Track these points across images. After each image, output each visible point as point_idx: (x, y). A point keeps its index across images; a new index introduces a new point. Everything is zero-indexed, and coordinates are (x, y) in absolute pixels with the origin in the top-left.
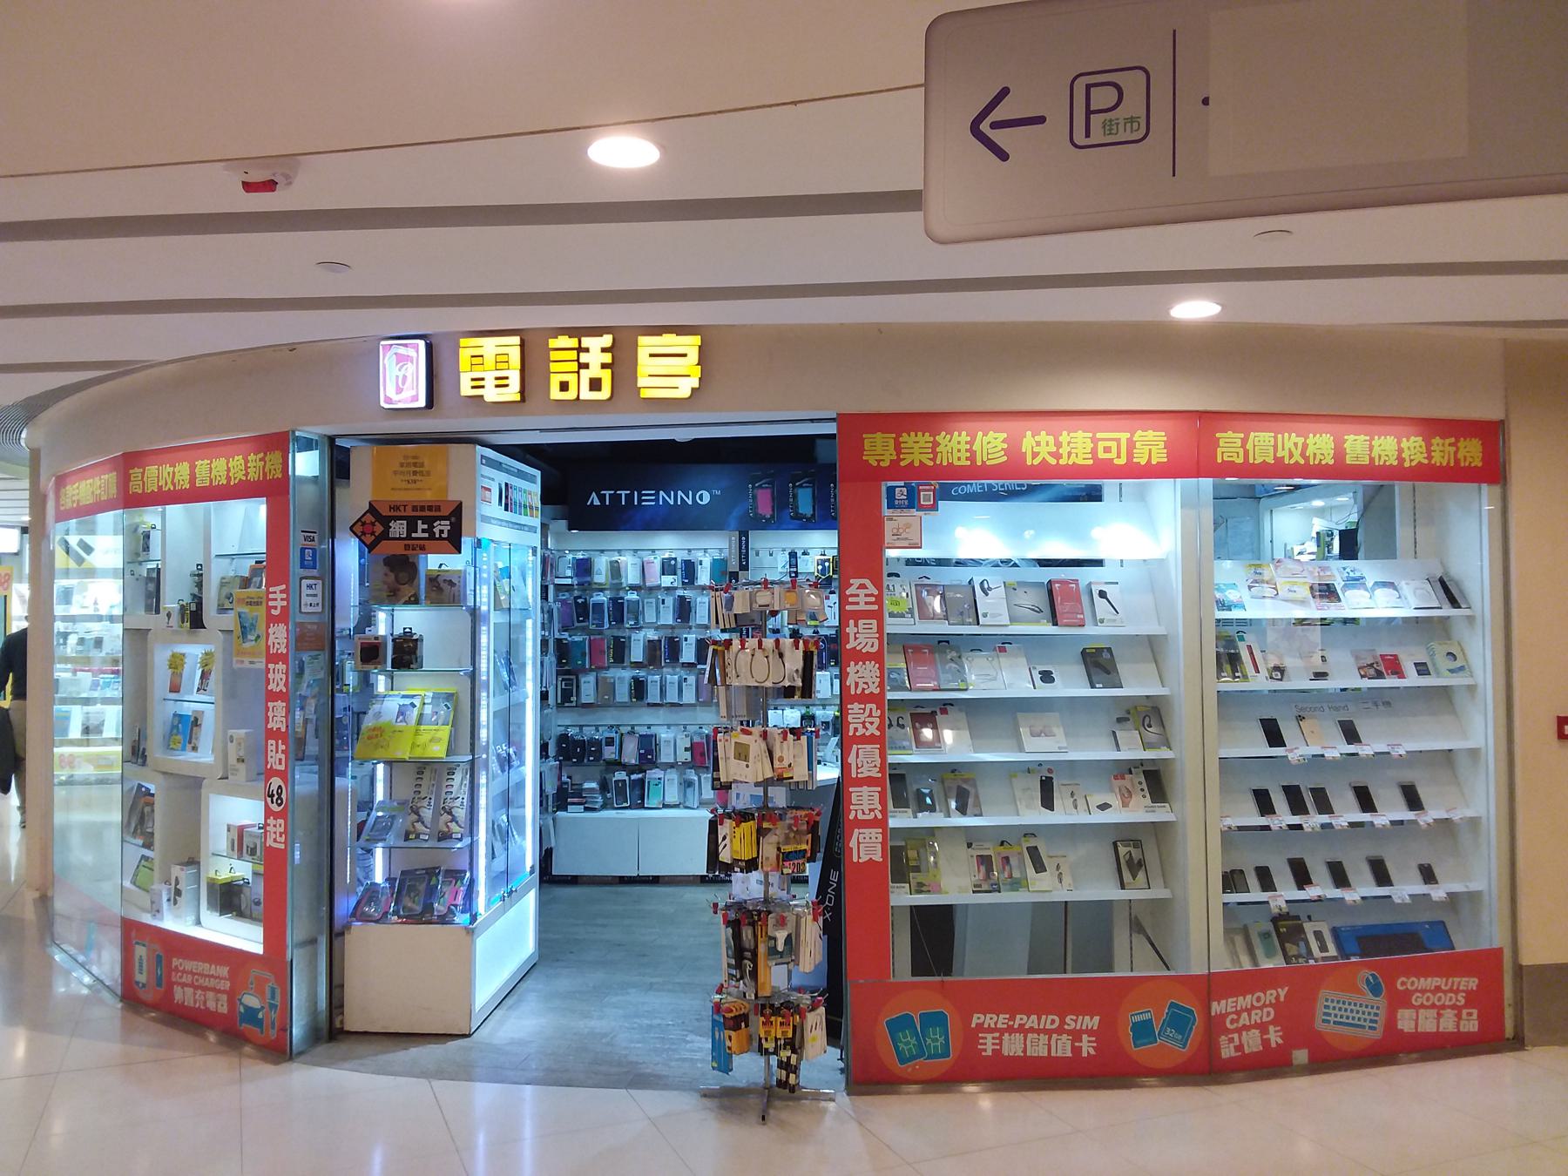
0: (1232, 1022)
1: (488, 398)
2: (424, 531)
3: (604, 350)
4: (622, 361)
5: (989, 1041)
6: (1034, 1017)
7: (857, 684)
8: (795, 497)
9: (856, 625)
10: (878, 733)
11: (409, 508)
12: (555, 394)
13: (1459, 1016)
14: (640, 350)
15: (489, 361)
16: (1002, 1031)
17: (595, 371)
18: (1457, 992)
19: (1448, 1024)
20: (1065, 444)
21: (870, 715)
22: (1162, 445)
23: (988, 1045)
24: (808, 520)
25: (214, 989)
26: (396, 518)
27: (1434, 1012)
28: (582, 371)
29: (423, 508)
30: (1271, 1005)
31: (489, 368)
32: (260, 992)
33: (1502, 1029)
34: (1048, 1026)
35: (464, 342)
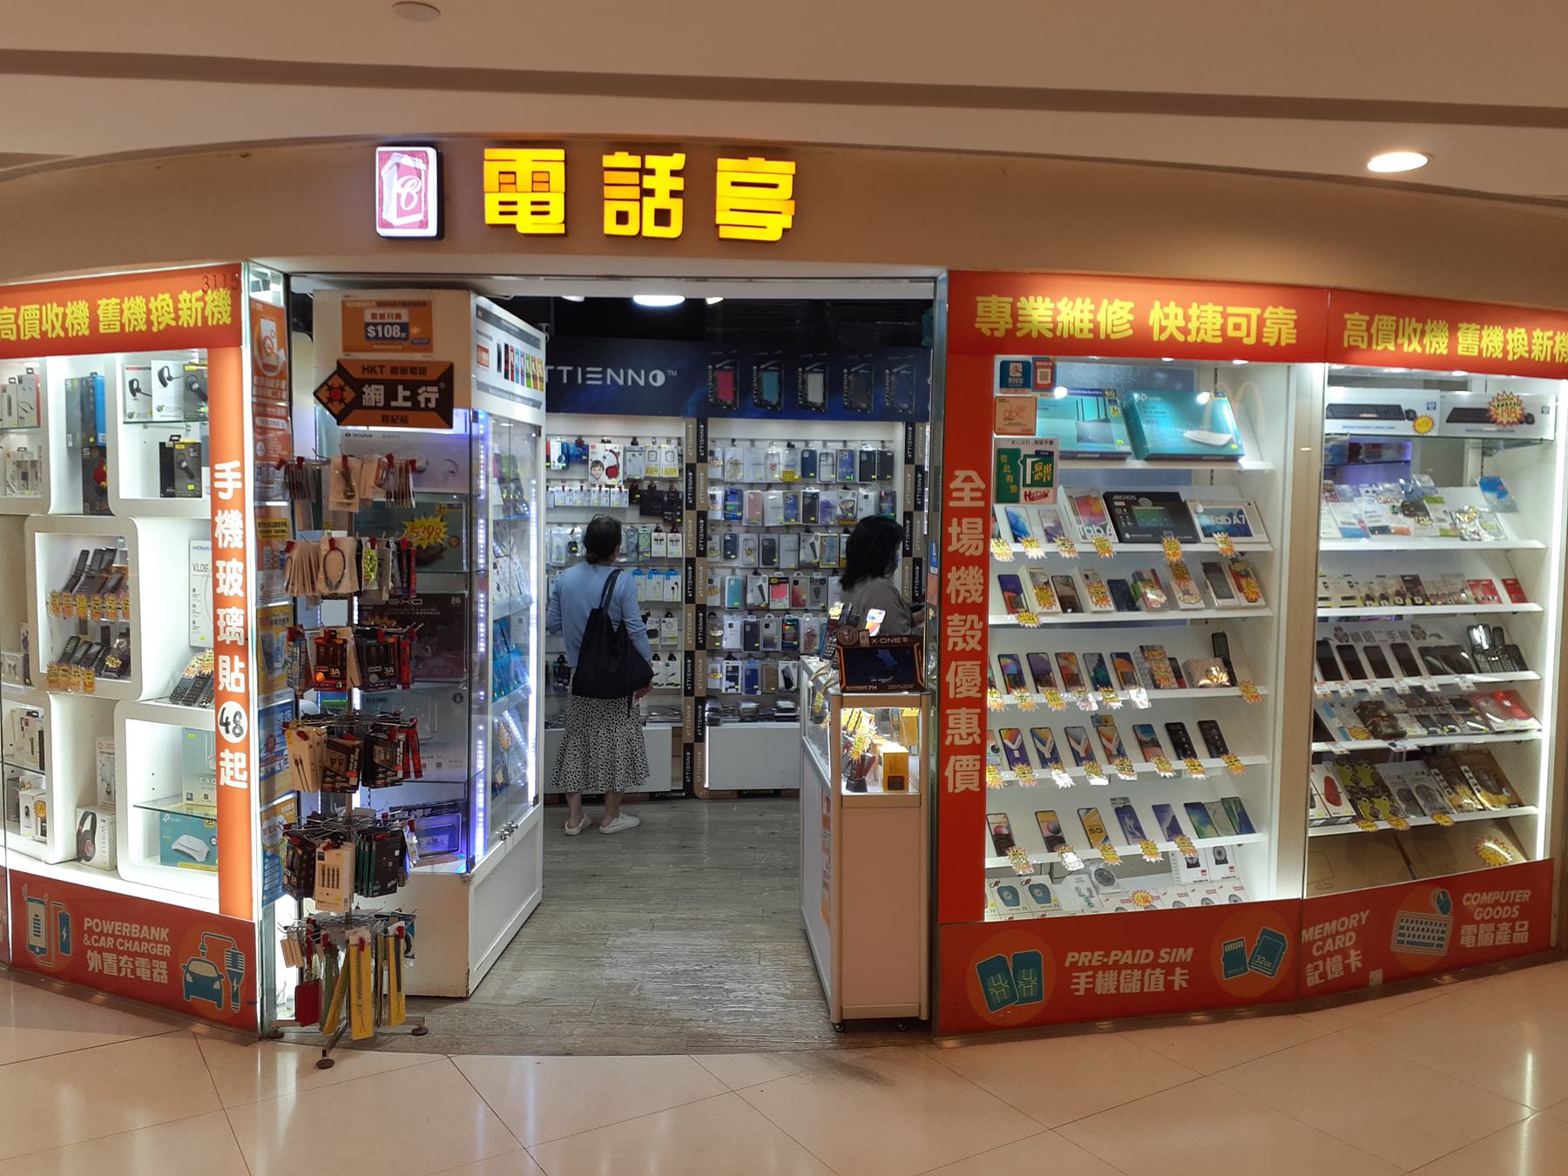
0: (1319, 948)
1: (521, 229)
2: (405, 399)
3: (674, 173)
4: (698, 192)
5: (1083, 980)
6: (1129, 953)
7: (958, 592)
8: (759, 381)
9: (960, 524)
10: (979, 648)
11: (387, 371)
12: (611, 227)
13: (1512, 928)
14: (719, 175)
15: (524, 180)
16: (1095, 969)
17: (662, 200)
18: (1512, 905)
19: (1503, 938)
20: (1194, 319)
21: (972, 628)
22: (1292, 324)
23: (1081, 984)
24: (774, 407)
25: (143, 955)
26: (371, 382)
27: (1491, 926)
28: (646, 200)
29: (404, 370)
30: (1353, 929)
31: (525, 189)
32: (215, 957)
33: (1549, 941)
34: (1143, 961)
35: (490, 153)
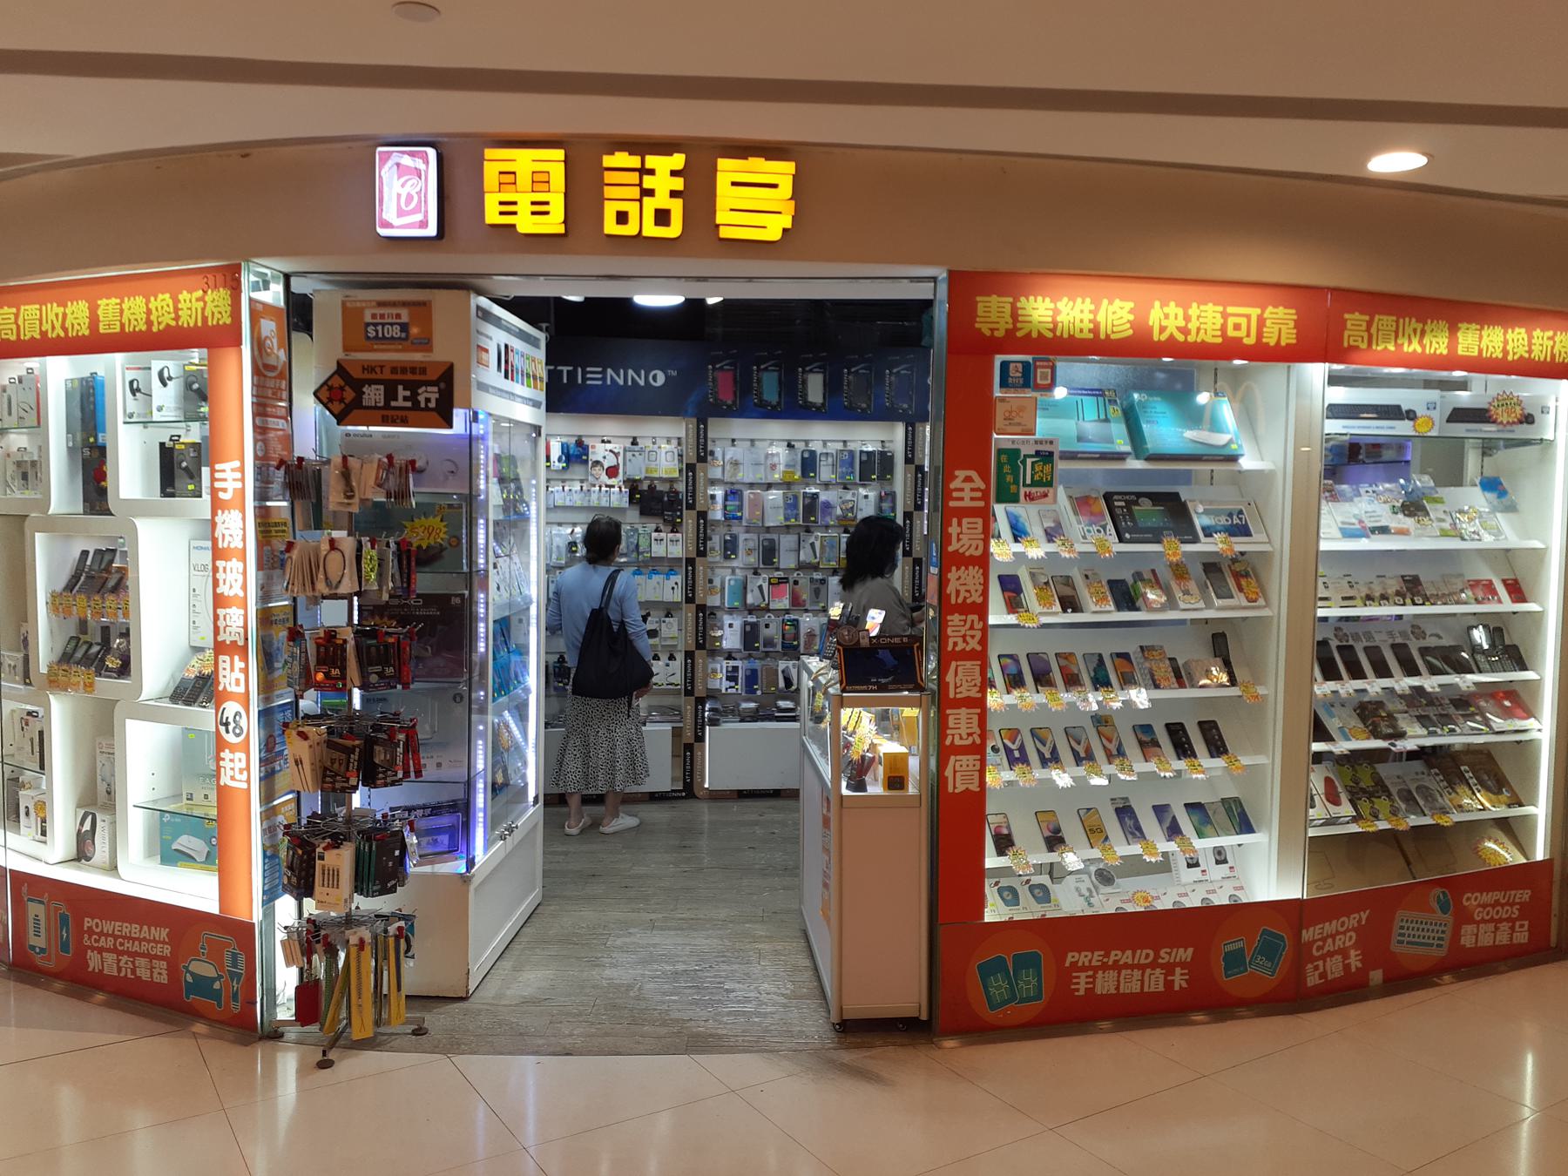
0: (1319, 948)
1: (521, 229)
2: (405, 399)
3: (674, 173)
4: (698, 192)
5: (1083, 980)
6: (1129, 953)
7: (958, 592)
8: (759, 381)
9: (960, 524)
10: (979, 648)
11: (387, 371)
12: (611, 227)
13: (1512, 928)
14: (719, 175)
15: (524, 180)
16: (1095, 969)
17: (662, 200)
18: (1512, 905)
19: (1503, 938)
20: (1194, 319)
21: (972, 628)
22: (1292, 324)
23: (1081, 984)
24: (774, 407)
25: (143, 955)
26: (371, 382)
27: (1491, 926)
28: (646, 200)
29: (404, 370)
30: (1353, 929)
31: (525, 189)
32: (215, 957)
33: (1549, 941)
34: (1143, 961)
35: (490, 153)
